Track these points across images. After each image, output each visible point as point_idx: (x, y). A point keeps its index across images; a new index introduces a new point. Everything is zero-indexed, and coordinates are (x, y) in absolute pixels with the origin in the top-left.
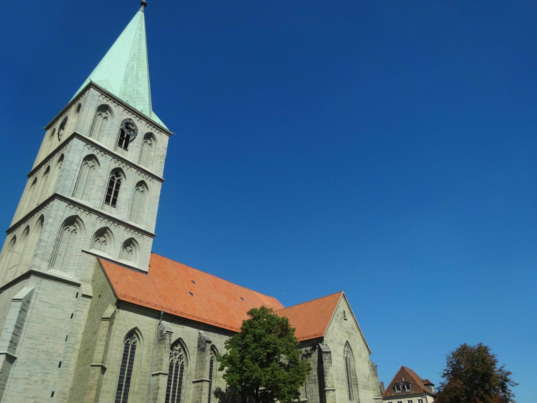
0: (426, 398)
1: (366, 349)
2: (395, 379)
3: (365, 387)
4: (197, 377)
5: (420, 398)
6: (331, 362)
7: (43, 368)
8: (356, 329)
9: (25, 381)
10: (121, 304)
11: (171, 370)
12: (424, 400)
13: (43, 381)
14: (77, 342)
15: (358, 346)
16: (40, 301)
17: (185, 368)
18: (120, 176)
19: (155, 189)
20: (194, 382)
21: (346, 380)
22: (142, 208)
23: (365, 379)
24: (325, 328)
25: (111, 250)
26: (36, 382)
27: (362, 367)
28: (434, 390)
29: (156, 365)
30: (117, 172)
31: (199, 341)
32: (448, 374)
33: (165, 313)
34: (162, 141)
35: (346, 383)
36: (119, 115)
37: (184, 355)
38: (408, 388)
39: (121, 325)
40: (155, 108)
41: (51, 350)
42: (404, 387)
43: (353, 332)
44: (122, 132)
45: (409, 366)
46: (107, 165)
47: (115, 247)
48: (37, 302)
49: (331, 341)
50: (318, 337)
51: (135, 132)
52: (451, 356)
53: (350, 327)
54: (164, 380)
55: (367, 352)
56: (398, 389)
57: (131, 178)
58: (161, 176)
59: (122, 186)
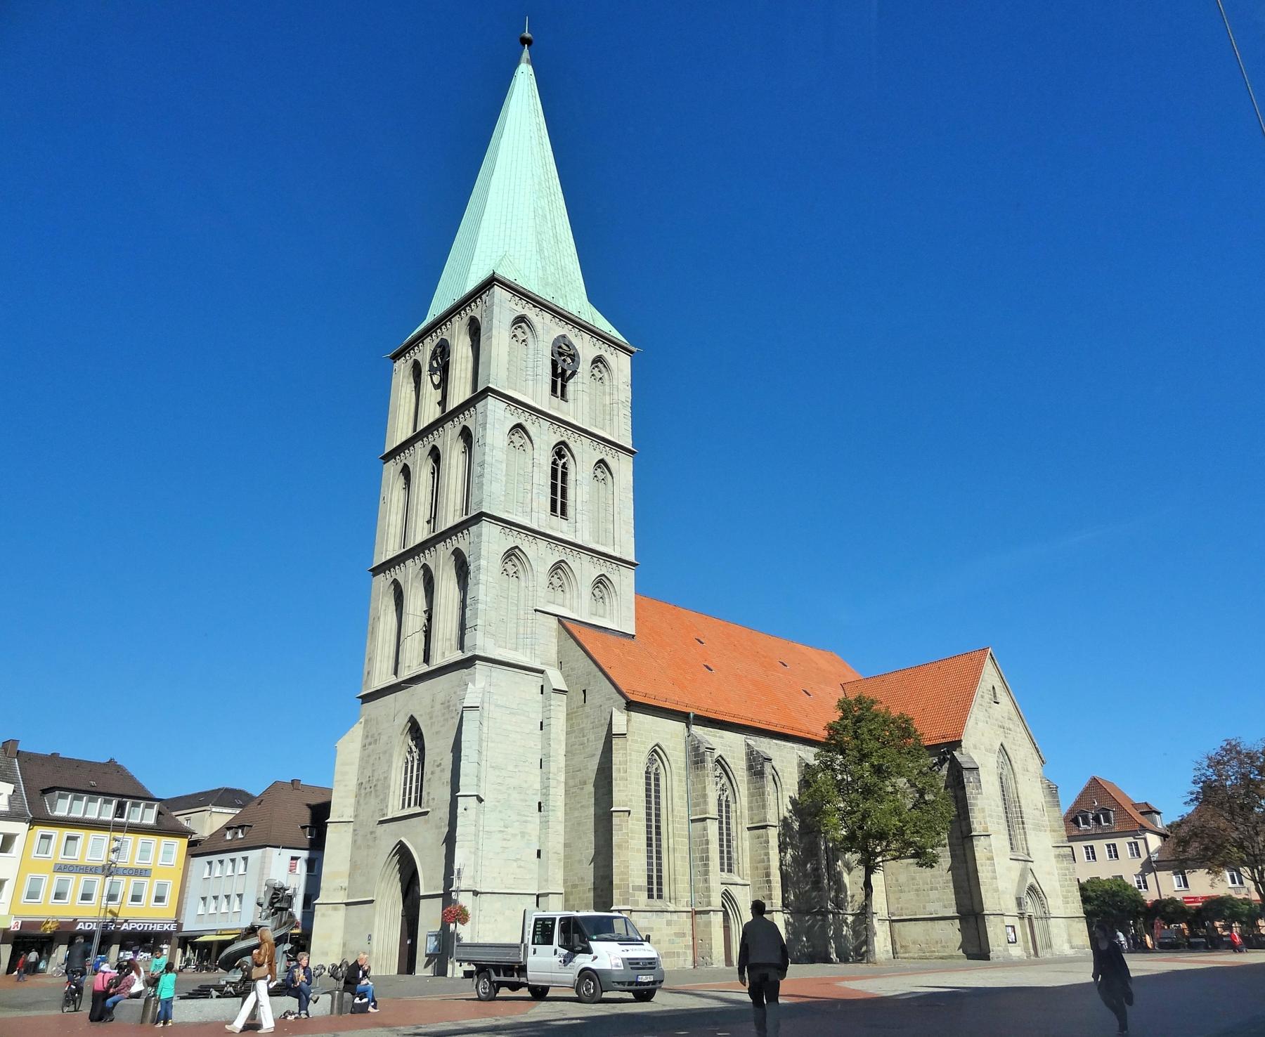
0: (1145, 839)
1: (1036, 756)
2: (1077, 803)
3: (1038, 827)
4: (756, 819)
5: (1131, 839)
6: (979, 787)
7: (519, 814)
8: (1016, 718)
9: (500, 835)
10: (631, 706)
11: (720, 811)
12: (1141, 843)
13: (523, 834)
14: (559, 771)
15: (1023, 753)
16: (497, 706)
17: (732, 806)
18: (563, 457)
19: (623, 467)
20: (749, 829)
21: (1003, 815)
22: (607, 511)
23: (1037, 813)
24: (962, 723)
25: (580, 606)
26: (514, 835)
27: (1031, 793)
28: (1161, 823)
29: (696, 805)
30: (560, 450)
31: (749, 760)
32: (1197, 799)
33: (695, 716)
34: (621, 364)
35: (1003, 821)
36: (548, 330)
37: (728, 784)
38: (1107, 820)
39: (636, 741)
40: (594, 296)
41: (525, 785)
42: (1097, 819)
43: (1011, 726)
44: (554, 364)
45: (1103, 775)
46: (545, 437)
47: (579, 596)
48: (492, 708)
49: (975, 747)
50: (949, 740)
51: (574, 357)
52: (1206, 763)
53: (1006, 715)
54: (713, 827)
55: (1038, 761)
56: (1086, 822)
57: (584, 455)
58: (627, 442)
59: (571, 477)
